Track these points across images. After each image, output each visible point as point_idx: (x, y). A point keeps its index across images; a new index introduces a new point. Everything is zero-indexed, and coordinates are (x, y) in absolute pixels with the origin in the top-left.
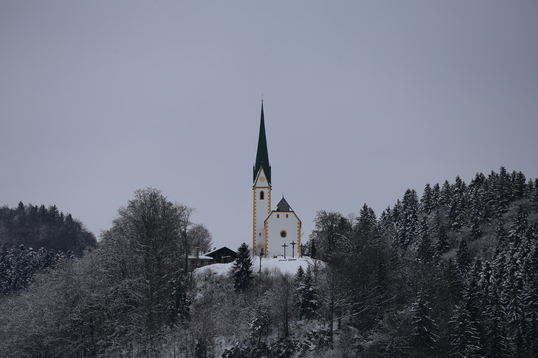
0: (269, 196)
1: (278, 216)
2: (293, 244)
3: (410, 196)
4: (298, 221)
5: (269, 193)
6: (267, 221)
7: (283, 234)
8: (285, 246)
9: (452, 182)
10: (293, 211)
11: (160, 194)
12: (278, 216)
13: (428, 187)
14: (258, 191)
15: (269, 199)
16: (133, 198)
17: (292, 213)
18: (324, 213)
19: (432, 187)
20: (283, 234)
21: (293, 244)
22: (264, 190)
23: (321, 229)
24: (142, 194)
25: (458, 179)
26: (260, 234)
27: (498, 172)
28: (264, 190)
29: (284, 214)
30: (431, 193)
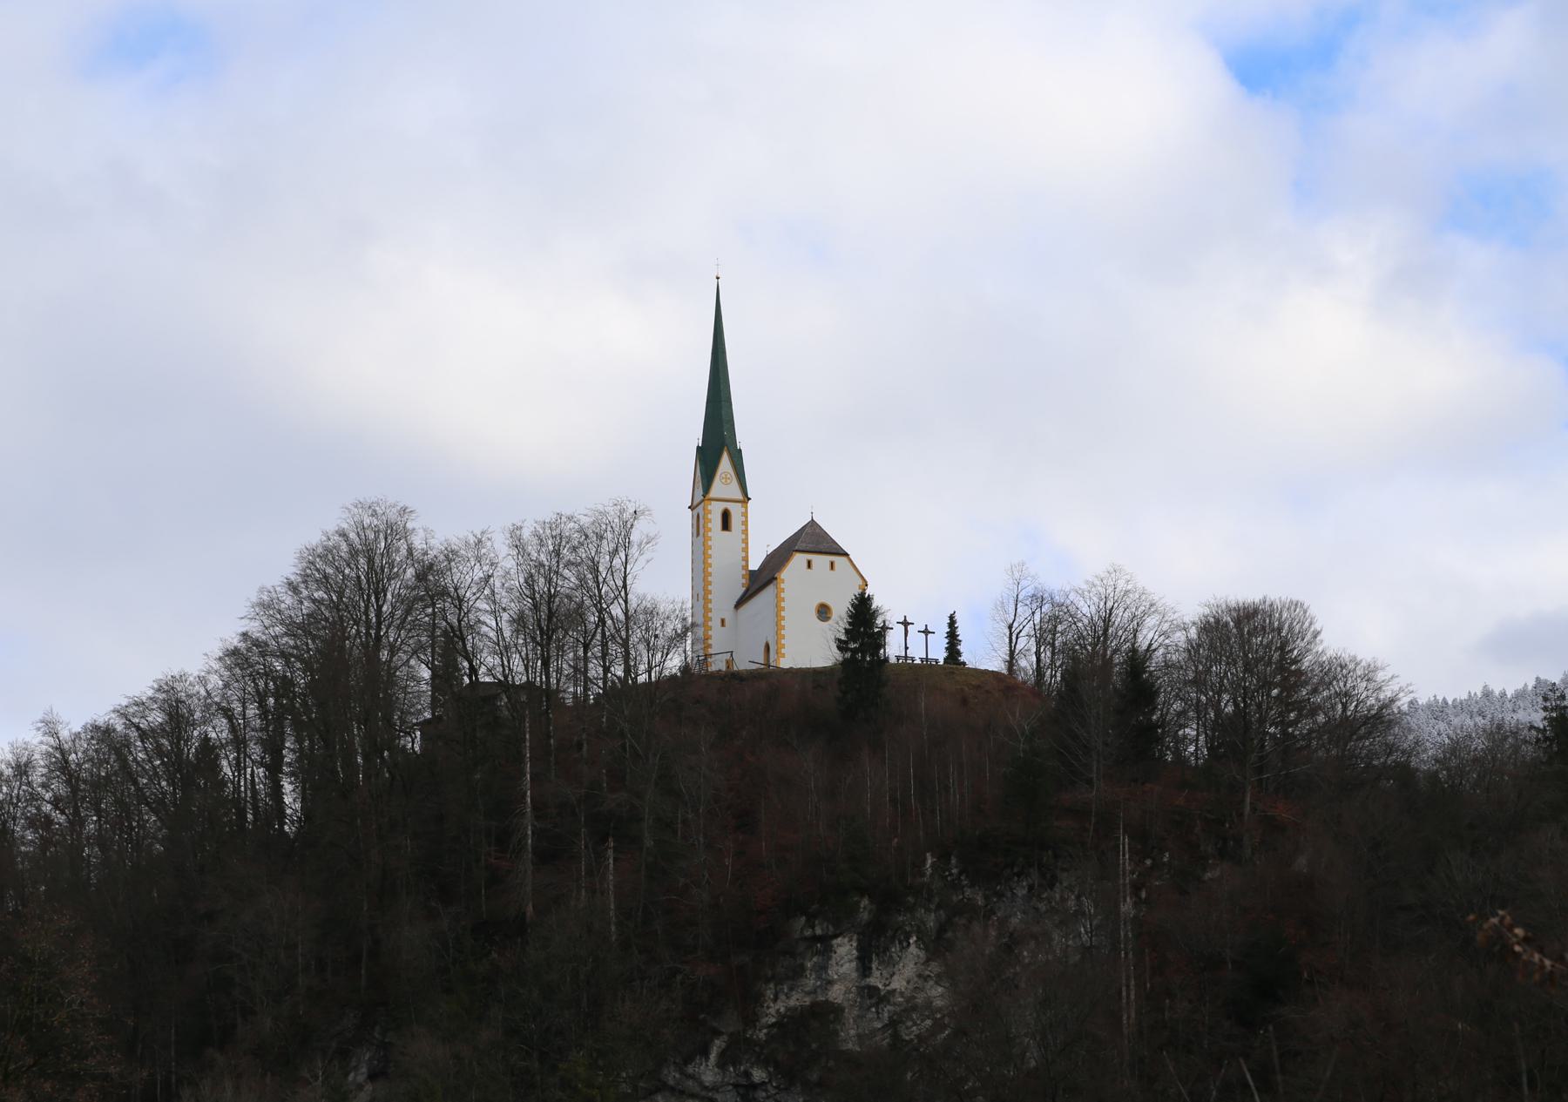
0: (745, 523)
1: (809, 564)
5: (745, 514)
10: (846, 555)
12: (809, 564)
14: (716, 510)
15: (745, 532)
17: (844, 559)
26: (723, 621)
29: (828, 558)
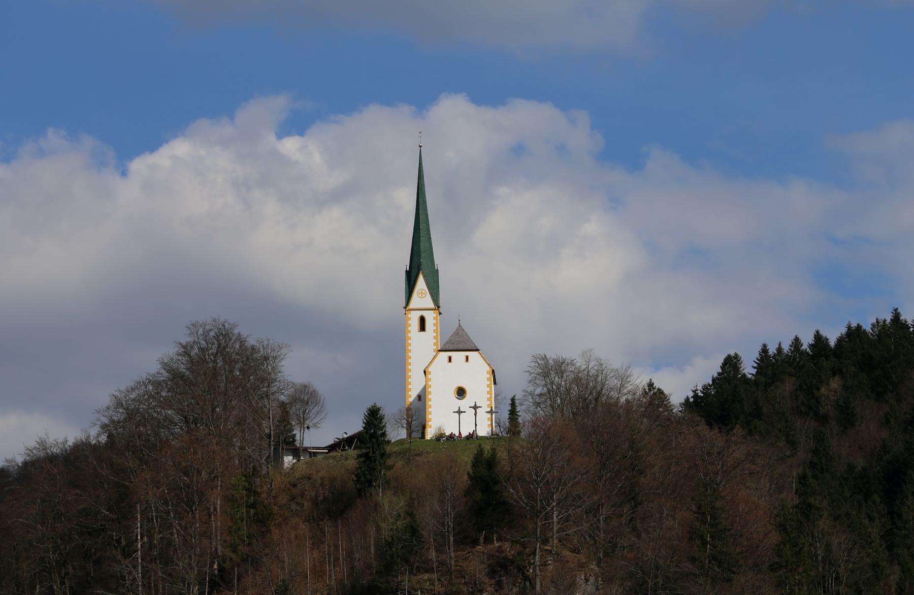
1: (450, 359)
2: (475, 408)
3: (731, 363)
4: (488, 369)
6: (430, 369)
7: (461, 392)
8: (459, 412)
9: (807, 340)
11: (236, 331)
12: (450, 359)
13: (765, 350)
16: (185, 339)
18: (545, 358)
19: (772, 350)
20: (461, 392)
21: (475, 408)
22: (424, 313)
23: (538, 391)
24: (201, 332)
25: (818, 336)
27: (888, 318)
28: (424, 313)
30: (769, 363)
